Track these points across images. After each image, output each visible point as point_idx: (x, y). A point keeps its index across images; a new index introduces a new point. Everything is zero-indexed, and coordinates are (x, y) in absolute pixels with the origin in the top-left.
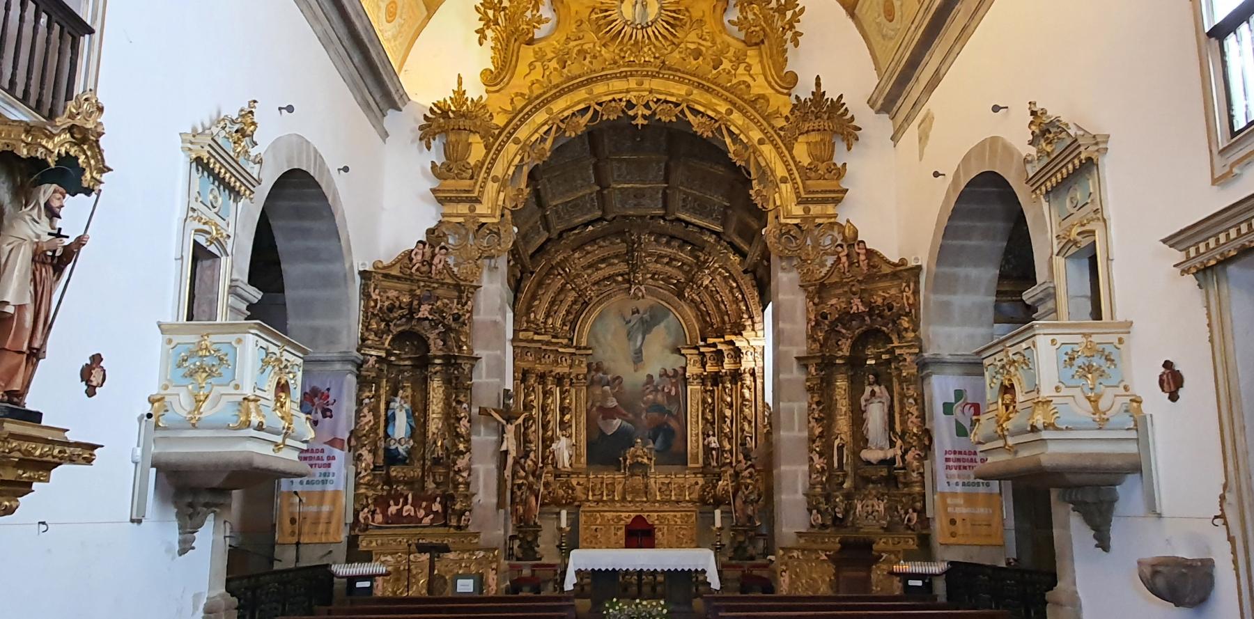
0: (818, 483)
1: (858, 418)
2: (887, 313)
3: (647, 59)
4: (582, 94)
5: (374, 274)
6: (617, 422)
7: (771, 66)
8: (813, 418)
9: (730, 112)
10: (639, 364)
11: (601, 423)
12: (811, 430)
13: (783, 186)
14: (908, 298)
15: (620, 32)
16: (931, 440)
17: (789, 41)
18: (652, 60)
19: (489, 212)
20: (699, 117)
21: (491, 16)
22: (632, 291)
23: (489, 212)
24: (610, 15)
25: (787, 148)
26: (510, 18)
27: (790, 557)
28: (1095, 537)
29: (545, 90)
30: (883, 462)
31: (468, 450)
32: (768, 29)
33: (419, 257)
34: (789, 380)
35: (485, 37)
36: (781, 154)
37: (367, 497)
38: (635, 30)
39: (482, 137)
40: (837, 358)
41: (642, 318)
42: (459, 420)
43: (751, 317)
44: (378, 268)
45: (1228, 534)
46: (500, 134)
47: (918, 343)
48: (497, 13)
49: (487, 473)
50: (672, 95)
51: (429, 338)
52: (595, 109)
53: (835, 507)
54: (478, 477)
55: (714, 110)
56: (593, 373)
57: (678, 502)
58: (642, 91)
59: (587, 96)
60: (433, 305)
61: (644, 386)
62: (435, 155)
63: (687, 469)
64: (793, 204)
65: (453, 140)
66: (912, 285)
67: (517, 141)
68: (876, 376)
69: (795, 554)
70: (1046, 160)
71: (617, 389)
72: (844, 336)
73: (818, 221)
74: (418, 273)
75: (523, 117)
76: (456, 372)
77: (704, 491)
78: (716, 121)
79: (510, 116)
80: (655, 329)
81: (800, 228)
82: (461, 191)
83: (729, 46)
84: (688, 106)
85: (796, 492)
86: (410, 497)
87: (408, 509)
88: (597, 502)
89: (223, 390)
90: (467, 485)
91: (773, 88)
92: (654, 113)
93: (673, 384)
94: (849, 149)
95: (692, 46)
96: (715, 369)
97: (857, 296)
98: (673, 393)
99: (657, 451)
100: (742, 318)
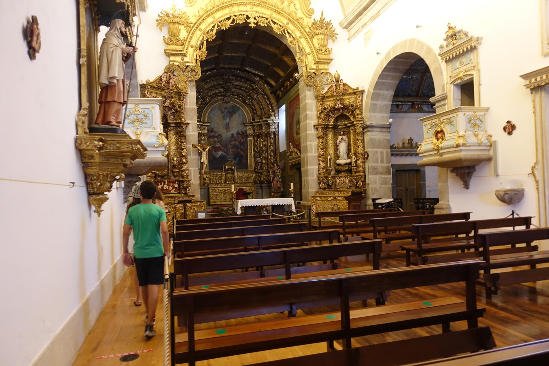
0: (322, 173)
1: (336, 148)
2: (351, 108)
5: (147, 86)
6: (220, 153)
7: (304, 5)
8: (320, 148)
9: (288, 24)
10: (228, 130)
11: (214, 153)
12: (319, 153)
14: (359, 102)
16: (368, 155)
20: (276, 24)
22: (225, 100)
23: (190, 61)
25: (311, 40)
27: (316, 200)
28: (464, 184)
29: (213, 7)
30: (346, 164)
31: (187, 162)
33: (165, 79)
34: (311, 134)
36: (308, 43)
40: (339, 126)
41: (229, 111)
42: (182, 149)
43: (273, 111)
44: (148, 83)
46: (194, 26)
47: (362, 119)
49: (194, 171)
50: (265, 14)
51: (167, 115)
52: (233, 18)
53: (329, 181)
54: (191, 174)
55: (282, 23)
56: (210, 133)
57: (246, 183)
58: (253, 11)
60: (171, 100)
61: (231, 138)
62: (165, 33)
63: (248, 170)
64: (312, 64)
65: (173, 27)
66: (361, 97)
67: (200, 30)
68: (344, 132)
69: (318, 199)
70: (451, 47)
71: (220, 140)
72: (332, 117)
73: (322, 71)
74: (164, 86)
76: (180, 129)
77: (256, 179)
78: (283, 27)
79: (198, 18)
80: (234, 115)
81: (315, 74)
82: (178, 51)
84: (271, 20)
85: (314, 176)
86: (166, 181)
87: (166, 187)
88: (215, 184)
89: (148, 130)
90: (187, 176)
91: (304, 15)
92: (258, 22)
93: (242, 138)
94: (333, 42)
96: (259, 132)
97: (339, 101)
98: (242, 141)
99: (236, 164)
100: (270, 111)
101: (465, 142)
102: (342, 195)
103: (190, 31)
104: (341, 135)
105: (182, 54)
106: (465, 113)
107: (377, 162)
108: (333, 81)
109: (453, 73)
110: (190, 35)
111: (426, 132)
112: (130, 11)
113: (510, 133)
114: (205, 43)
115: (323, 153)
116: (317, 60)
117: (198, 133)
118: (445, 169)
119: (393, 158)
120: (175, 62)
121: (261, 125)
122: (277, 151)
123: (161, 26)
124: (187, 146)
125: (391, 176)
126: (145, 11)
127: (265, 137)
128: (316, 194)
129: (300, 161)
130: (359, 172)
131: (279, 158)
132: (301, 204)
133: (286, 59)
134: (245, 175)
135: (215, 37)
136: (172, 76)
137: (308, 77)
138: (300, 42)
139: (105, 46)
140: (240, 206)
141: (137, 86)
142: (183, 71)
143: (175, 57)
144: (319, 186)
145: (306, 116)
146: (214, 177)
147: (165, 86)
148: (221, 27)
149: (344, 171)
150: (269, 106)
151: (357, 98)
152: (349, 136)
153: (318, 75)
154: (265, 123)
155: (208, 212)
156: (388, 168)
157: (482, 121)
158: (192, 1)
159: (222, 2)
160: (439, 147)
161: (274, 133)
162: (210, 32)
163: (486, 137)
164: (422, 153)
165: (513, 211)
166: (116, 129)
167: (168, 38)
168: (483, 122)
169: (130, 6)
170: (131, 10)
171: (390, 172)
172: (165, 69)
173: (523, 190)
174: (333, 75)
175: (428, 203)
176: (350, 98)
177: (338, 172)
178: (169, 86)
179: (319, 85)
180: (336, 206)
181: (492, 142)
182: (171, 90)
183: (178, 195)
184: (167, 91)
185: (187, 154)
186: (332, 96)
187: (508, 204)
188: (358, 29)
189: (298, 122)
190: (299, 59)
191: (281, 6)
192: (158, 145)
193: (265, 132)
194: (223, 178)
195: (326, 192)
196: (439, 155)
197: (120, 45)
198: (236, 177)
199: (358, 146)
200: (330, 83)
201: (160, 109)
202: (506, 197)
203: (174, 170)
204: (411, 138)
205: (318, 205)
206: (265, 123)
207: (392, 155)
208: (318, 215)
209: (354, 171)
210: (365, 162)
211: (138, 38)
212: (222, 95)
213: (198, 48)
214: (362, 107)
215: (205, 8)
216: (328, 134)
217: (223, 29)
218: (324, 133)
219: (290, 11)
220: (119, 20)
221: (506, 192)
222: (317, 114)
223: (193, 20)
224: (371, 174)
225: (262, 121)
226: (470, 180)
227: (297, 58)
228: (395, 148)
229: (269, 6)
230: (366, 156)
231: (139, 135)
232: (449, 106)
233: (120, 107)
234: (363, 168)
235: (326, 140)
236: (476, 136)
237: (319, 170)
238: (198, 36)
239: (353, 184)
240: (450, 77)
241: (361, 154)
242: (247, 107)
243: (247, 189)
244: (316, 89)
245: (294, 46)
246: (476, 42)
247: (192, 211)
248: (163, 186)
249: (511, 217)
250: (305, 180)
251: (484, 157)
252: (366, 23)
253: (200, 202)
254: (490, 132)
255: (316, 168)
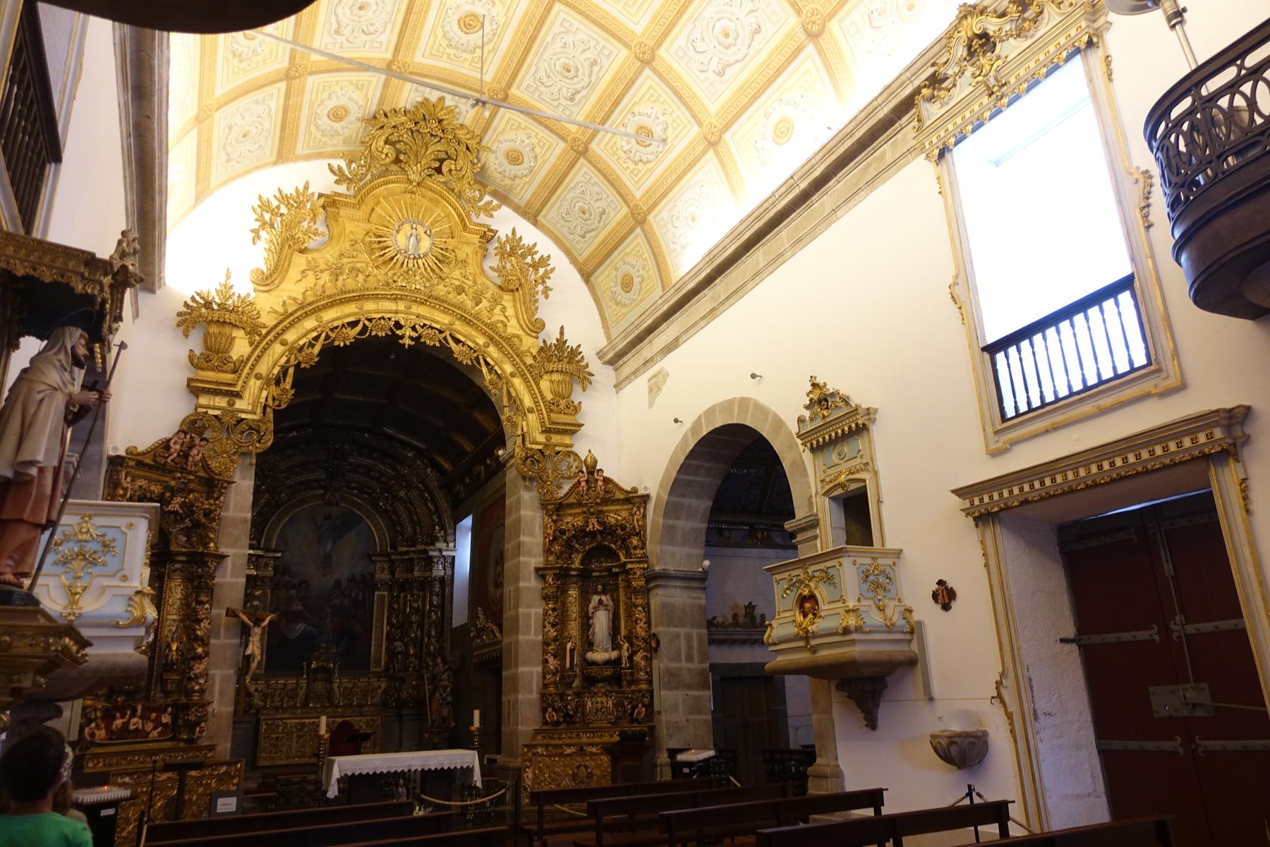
0: (552, 683)
3: (418, 287)
4: (351, 308)
5: (127, 460)
6: (301, 626)
8: (549, 623)
9: (487, 345)
12: (545, 634)
13: (530, 416)
14: (638, 521)
15: (392, 258)
16: (658, 642)
17: (540, 293)
18: (423, 289)
19: (250, 408)
20: (460, 345)
21: (268, 220)
22: (327, 497)
23: (250, 408)
24: (385, 241)
26: (286, 225)
27: (534, 754)
28: (865, 718)
30: (608, 663)
31: (207, 654)
32: (523, 281)
33: (178, 447)
35: (259, 237)
37: (96, 710)
38: (406, 260)
39: (247, 333)
42: (199, 621)
44: (132, 453)
45: (1006, 710)
47: (644, 559)
48: (273, 217)
50: (437, 322)
51: (171, 533)
52: (364, 324)
53: (567, 704)
54: (213, 685)
55: (474, 342)
57: (360, 706)
59: (357, 310)
62: (195, 343)
67: (284, 343)
68: (604, 586)
70: (819, 422)
72: (577, 551)
73: (558, 449)
75: (293, 321)
76: (200, 570)
78: (475, 352)
81: (542, 453)
82: (222, 384)
83: (488, 288)
84: (450, 335)
85: (531, 692)
86: (139, 708)
87: (135, 723)
88: (277, 709)
89: (106, 582)
90: (202, 691)
92: (420, 337)
95: (457, 283)
96: (405, 576)
98: (360, 597)
100: (434, 529)
101: (861, 623)
102: (597, 740)
103: (260, 343)
104: (597, 593)
105: (232, 391)
106: (856, 559)
107: (678, 659)
108: (583, 472)
109: (826, 474)
110: (257, 352)
111: (780, 596)
112: (108, 310)
113: (946, 607)
114: (291, 370)
115: (556, 636)
116: (548, 425)
117: (249, 577)
118: (825, 682)
119: (713, 649)
120: (209, 408)
121: (411, 560)
122: (446, 625)
123: (188, 327)
124: (214, 612)
125: (709, 693)
126: (153, 291)
127: (418, 590)
128: (534, 738)
129: (501, 653)
130: (638, 682)
131: (449, 641)
132: (496, 764)
133: (479, 417)
134: (359, 684)
135: (316, 359)
136: (197, 441)
137: (527, 458)
138: (513, 386)
139: (24, 388)
140: (336, 774)
141: (101, 459)
142: (228, 429)
143: (212, 397)
144: (544, 717)
145: (518, 546)
146: (276, 690)
147: (176, 463)
148: (334, 341)
149: (604, 680)
150: (434, 517)
151: (634, 511)
152: (615, 595)
153: (549, 456)
154: (422, 556)
155: (247, 792)
156: (702, 673)
157: (890, 579)
158: (272, 282)
159: (341, 289)
160: (808, 631)
161: (442, 580)
162: (307, 348)
163: (900, 612)
164: (775, 644)
165: (969, 786)
166: (11, 593)
167: (201, 354)
168: (893, 580)
169: (109, 302)
170: (111, 309)
171: (708, 682)
172: (182, 424)
173: (985, 734)
174: (583, 459)
175: (793, 763)
176: (617, 510)
177: (589, 681)
178: (186, 463)
179: (551, 479)
180: (584, 769)
181: (913, 623)
182: (190, 473)
183: (169, 744)
184: (179, 475)
185: (209, 634)
186: (579, 504)
187: (959, 768)
188: (636, 367)
189: (501, 559)
190: (509, 419)
191: (473, 308)
192: (127, 622)
193: (419, 577)
194: (301, 693)
195: (560, 734)
196: (810, 650)
197: (65, 386)
198: (336, 690)
199: (636, 620)
200: (576, 475)
201: (150, 529)
202: (954, 750)
203: (165, 676)
204: (750, 603)
205: (540, 767)
206: (422, 556)
207: (712, 642)
208: (537, 798)
209: (627, 681)
210: (651, 659)
211: (123, 351)
212: (321, 487)
213: (273, 382)
214: (645, 531)
215: (300, 297)
216: (568, 590)
217: (339, 345)
218: (558, 588)
219: (493, 320)
220: (73, 329)
221: (953, 739)
222: (545, 543)
223: (268, 320)
224: (666, 689)
225: (413, 552)
226: (878, 709)
227: (503, 418)
228: (717, 626)
229: (446, 306)
230: (654, 645)
231: (78, 593)
232: (824, 539)
233: (34, 534)
234: (647, 673)
235: (564, 604)
236: (881, 609)
237: (544, 677)
238: (276, 356)
239: (624, 713)
240: (822, 481)
241: (643, 639)
242: (380, 516)
243: (360, 723)
244: (542, 487)
245: (497, 392)
246: (866, 417)
247: (201, 790)
248: (128, 722)
249: (967, 802)
250: (509, 702)
251: (901, 657)
252: (651, 359)
253: (229, 764)
254: (908, 603)
255: (538, 672)
